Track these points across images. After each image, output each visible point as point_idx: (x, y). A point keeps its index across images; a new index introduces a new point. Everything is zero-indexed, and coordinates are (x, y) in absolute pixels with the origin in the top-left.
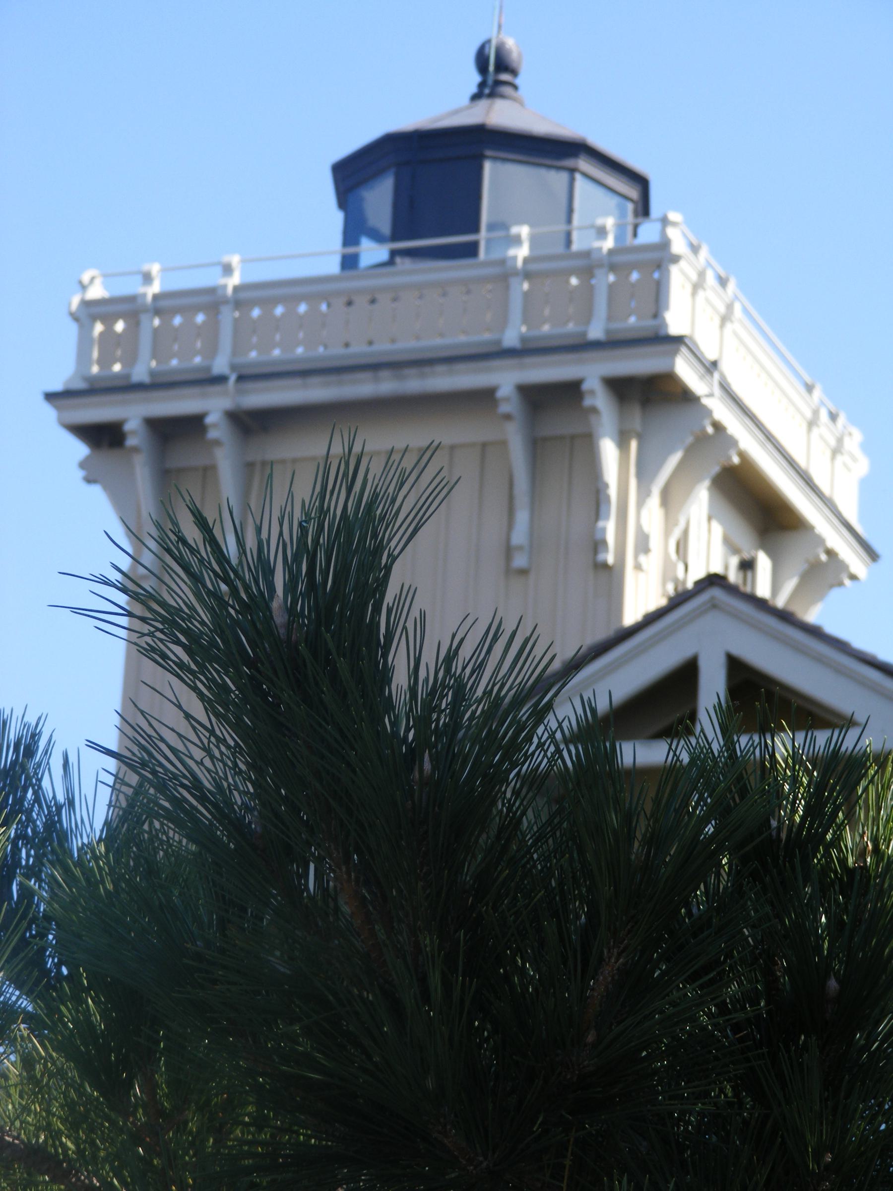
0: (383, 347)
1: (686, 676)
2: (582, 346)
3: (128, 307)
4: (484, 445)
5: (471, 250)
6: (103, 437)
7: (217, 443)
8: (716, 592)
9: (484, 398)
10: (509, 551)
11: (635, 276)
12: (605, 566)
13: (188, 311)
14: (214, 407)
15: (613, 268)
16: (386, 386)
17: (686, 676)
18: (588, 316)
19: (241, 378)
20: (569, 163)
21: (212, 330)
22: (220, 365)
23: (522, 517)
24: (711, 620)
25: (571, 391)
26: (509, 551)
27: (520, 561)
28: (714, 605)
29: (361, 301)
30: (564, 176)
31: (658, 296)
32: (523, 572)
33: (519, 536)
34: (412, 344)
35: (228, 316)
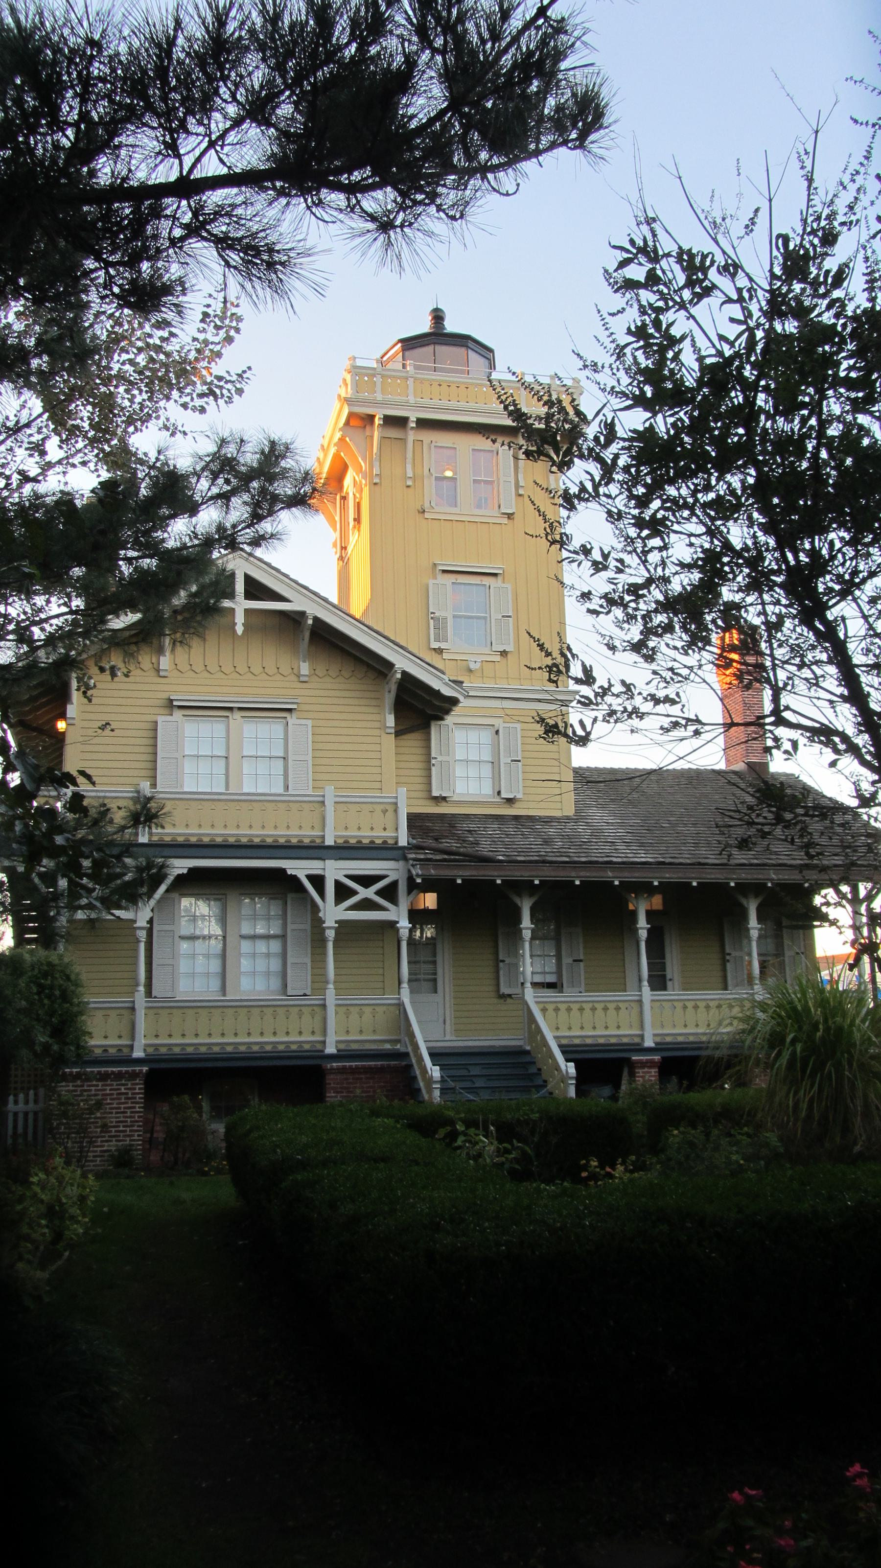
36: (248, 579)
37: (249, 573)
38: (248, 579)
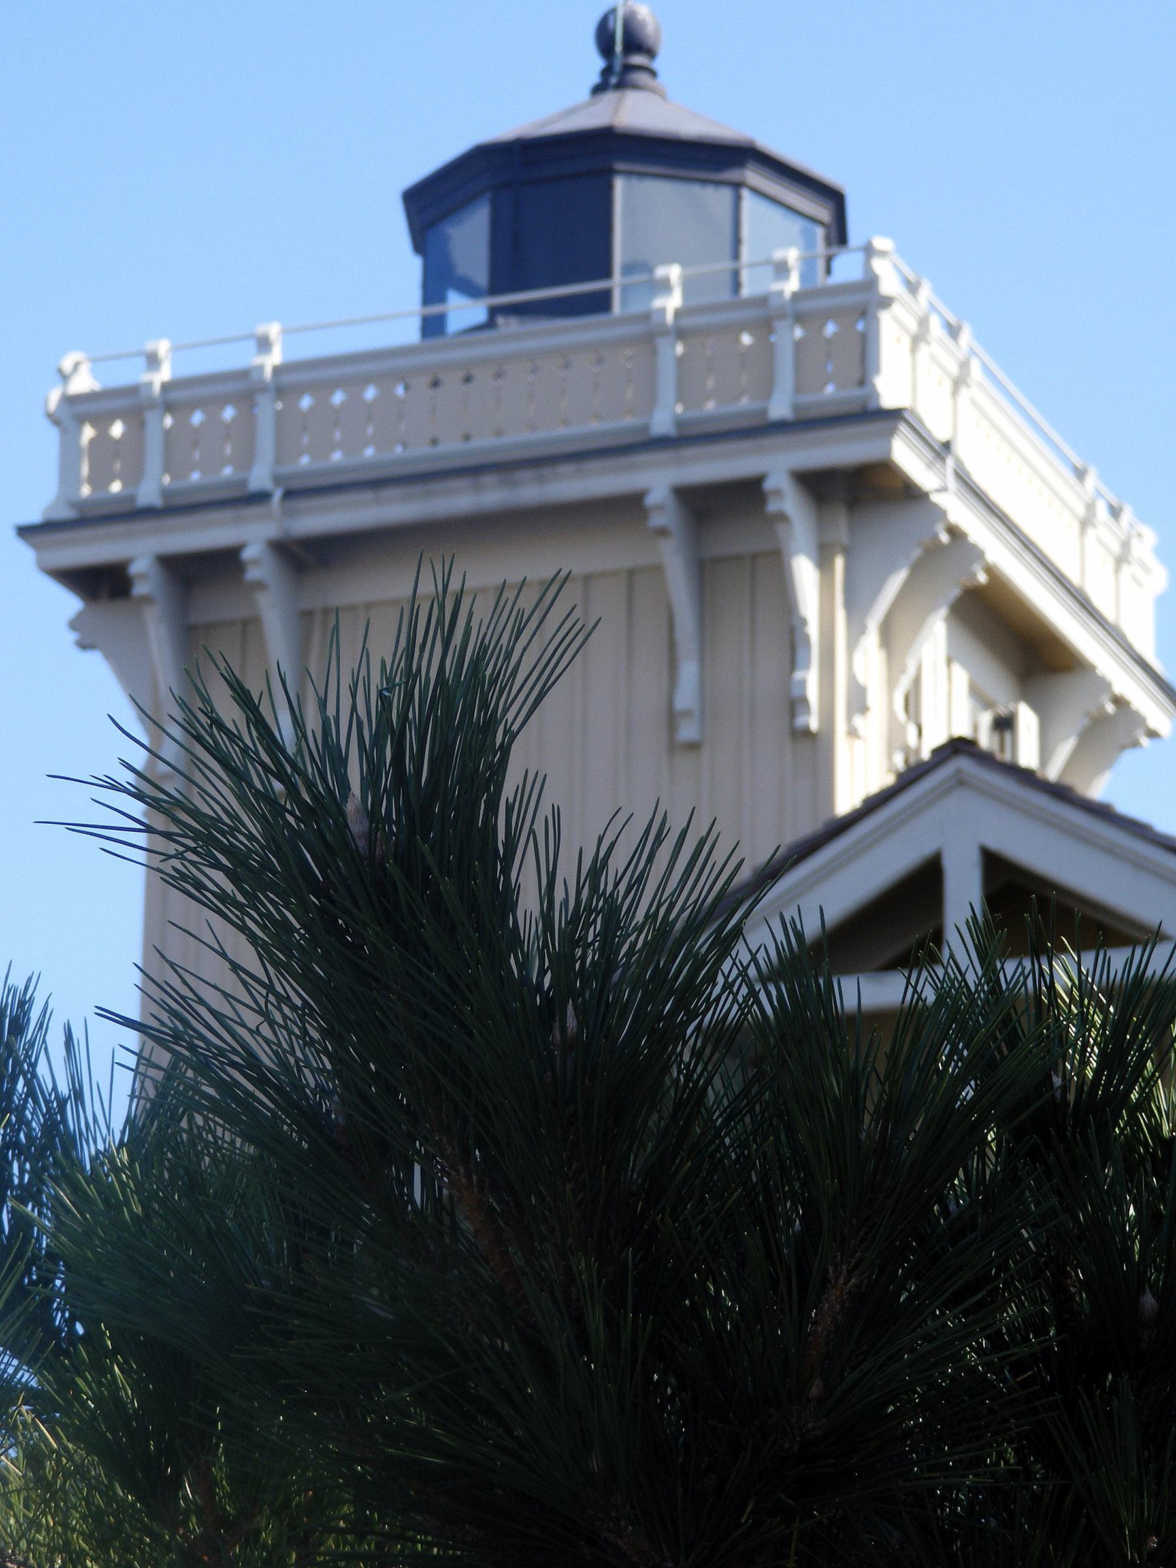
0: (484, 443)
1: (926, 881)
2: (762, 429)
3: (129, 403)
4: (631, 573)
5: (600, 303)
6: (100, 584)
7: (260, 585)
8: (963, 763)
9: (628, 507)
10: (672, 718)
11: (830, 329)
12: (807, 733)
13: (211, 404)
14: (253, 535)
15: (799, 318)
16: (491, 496)
17: (926, 881)
18: (767, 388)
19: (289, 494)
20: (732, 175)
21: (246, 430)
22: (260, 477)
23: (688, 670)
24: (958, 803)
25: (748, 493)
26: (672, 718)
27: (688, 731)
28: (960, 782)
29: (451, 381)
30: (726, 194)
31: (863, 356)
32: (693, 747)
33: (686, 697)
34: (525, 436)
35: (267, 408)
36: (994, 865)
37: (994, 845)
38: (994, 865)
